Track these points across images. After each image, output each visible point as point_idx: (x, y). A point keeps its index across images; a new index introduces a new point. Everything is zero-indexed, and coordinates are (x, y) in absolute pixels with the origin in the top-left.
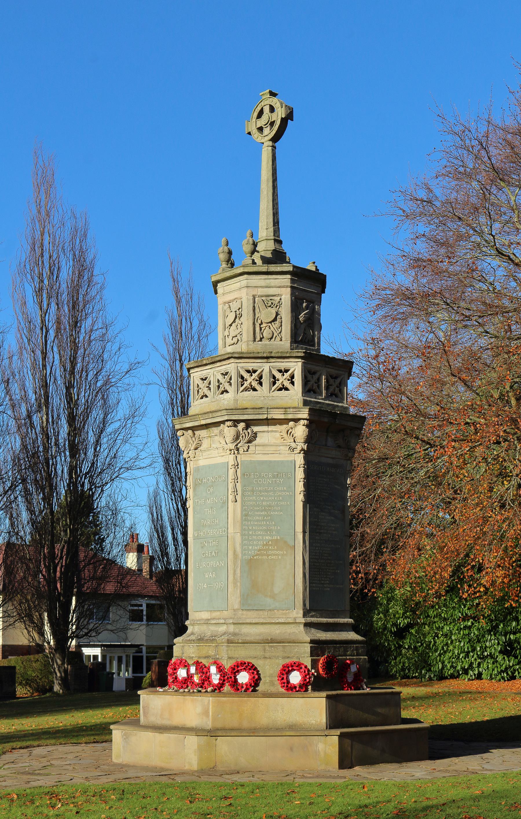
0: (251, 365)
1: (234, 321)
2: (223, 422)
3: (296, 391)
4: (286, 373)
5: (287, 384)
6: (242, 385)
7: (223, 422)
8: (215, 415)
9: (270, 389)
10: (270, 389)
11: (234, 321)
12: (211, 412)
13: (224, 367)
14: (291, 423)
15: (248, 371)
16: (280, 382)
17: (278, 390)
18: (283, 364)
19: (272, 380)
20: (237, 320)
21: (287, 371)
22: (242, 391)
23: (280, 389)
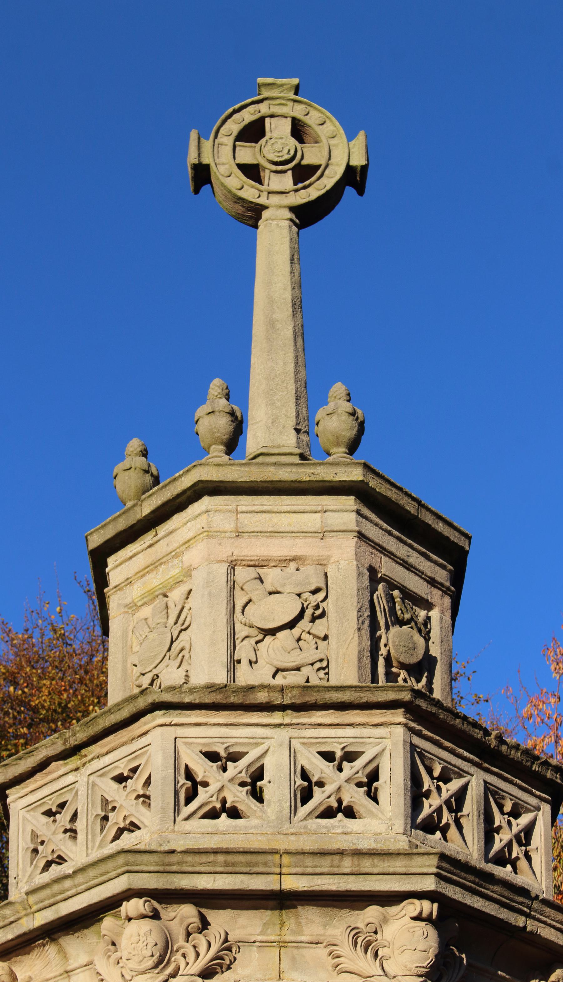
0: (217, 730)
1: (291, 625)
2: (111, 904)
3: (384, 821)
4: (351, 760)
5: (355, 796)
6: (189, 800)
7: (111, 904)
8: (367, 865)
9: (177, 809)
10: (177, 809)
11: (291, 625)
12: (358, 853)
13: (349, 732)
14: (373, 912)
15: (212, 756)
16: (329, 788)
17: (204, 816)
18: (340, 731)
19: (299, 782)
20: (304, 624)
21: (350, 757)
22: (187, 819)
23: (213, 814)
